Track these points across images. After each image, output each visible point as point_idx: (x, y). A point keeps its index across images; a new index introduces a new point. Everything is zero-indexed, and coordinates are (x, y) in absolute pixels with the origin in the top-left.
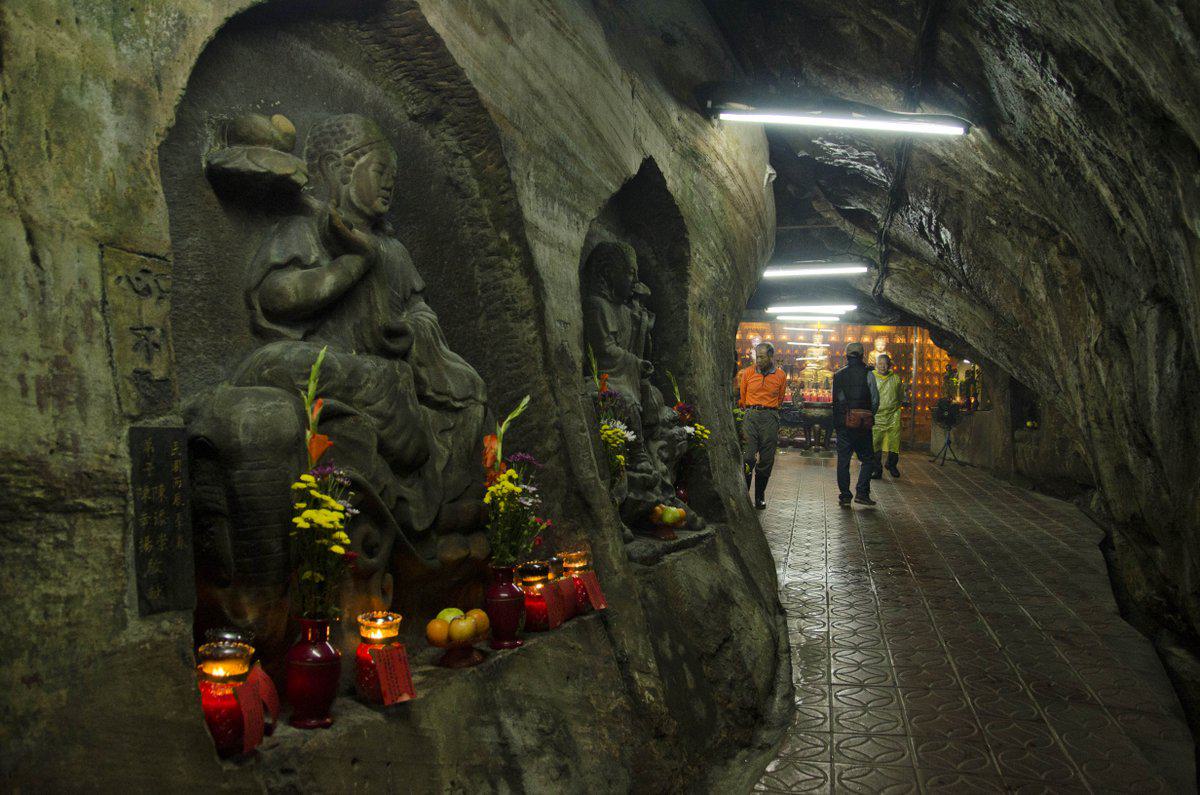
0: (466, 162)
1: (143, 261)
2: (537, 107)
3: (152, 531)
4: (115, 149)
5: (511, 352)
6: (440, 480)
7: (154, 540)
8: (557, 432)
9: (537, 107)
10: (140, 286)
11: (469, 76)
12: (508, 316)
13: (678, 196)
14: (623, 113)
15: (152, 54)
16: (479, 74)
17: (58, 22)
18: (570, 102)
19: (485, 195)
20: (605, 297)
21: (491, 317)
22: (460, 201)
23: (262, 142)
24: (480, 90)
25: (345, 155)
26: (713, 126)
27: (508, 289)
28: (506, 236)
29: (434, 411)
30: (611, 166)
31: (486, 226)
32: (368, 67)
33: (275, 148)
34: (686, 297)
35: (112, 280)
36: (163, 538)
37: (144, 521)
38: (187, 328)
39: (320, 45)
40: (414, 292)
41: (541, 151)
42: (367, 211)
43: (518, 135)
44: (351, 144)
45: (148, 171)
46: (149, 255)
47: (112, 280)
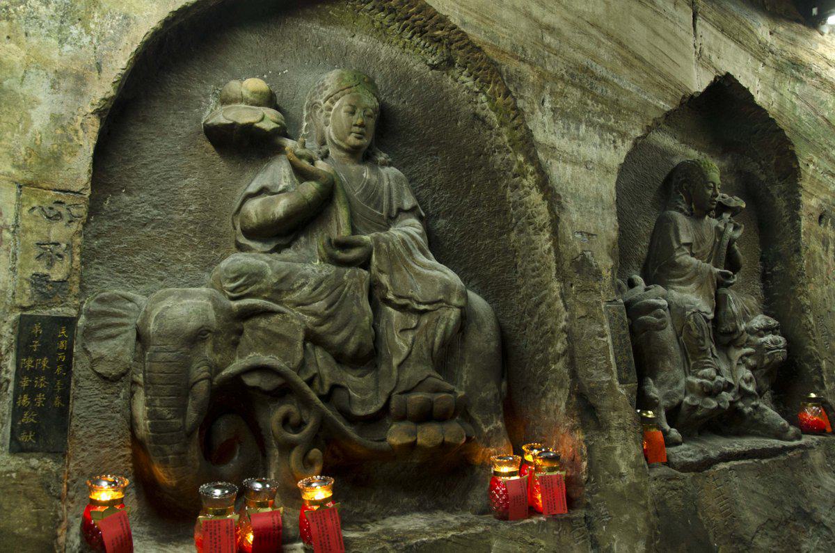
0: (483, 98)
1: (57, 195)
2: (548, 39)
3: (32, 391)
4: (47, 117)
5: (534, 261)
6: (395, 373)
7: (32, 398)
8: (565, 336)
9: (548, 39)
10: (52, 214)
11: (454, 20)
12: (530, 229)
13: (773, 110)
14: (675, 35)
15: (95, 48)
16: (467, 19)
17: (8, 37)
18: (593, 31)
19: (502, 124)
20: (681, 211)
21: (521, 231)
22: (488, 132)
23: (235, 101)
24: (469, 31)
25: (325, 102)
26: (822, 34)
27: (528, 205)
28: (521, 158)
29: (398, 312)
30: (659, 85)
31: (508, 151)
32: (381, 32)
33: (247, 103)
34: (798, 208)
35: (25, 210)
36: (40, 397)
37: (25, 383)
38: (177, 245)
39: (332, 22)
40: (400, 210)
41: (557, 78)
42: (344, 146)
43: (525, 68)
44: (327, 93)
45: (76, 131)
46: (64, 191)
47: (25, 210)
